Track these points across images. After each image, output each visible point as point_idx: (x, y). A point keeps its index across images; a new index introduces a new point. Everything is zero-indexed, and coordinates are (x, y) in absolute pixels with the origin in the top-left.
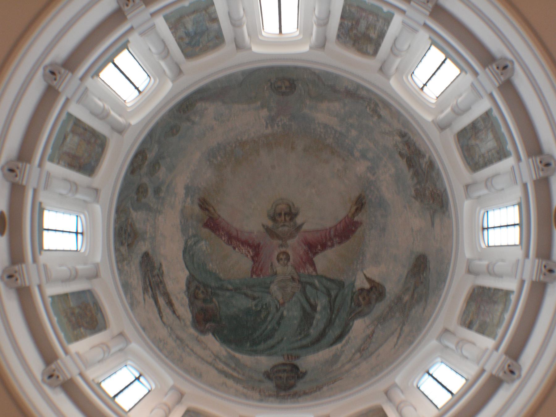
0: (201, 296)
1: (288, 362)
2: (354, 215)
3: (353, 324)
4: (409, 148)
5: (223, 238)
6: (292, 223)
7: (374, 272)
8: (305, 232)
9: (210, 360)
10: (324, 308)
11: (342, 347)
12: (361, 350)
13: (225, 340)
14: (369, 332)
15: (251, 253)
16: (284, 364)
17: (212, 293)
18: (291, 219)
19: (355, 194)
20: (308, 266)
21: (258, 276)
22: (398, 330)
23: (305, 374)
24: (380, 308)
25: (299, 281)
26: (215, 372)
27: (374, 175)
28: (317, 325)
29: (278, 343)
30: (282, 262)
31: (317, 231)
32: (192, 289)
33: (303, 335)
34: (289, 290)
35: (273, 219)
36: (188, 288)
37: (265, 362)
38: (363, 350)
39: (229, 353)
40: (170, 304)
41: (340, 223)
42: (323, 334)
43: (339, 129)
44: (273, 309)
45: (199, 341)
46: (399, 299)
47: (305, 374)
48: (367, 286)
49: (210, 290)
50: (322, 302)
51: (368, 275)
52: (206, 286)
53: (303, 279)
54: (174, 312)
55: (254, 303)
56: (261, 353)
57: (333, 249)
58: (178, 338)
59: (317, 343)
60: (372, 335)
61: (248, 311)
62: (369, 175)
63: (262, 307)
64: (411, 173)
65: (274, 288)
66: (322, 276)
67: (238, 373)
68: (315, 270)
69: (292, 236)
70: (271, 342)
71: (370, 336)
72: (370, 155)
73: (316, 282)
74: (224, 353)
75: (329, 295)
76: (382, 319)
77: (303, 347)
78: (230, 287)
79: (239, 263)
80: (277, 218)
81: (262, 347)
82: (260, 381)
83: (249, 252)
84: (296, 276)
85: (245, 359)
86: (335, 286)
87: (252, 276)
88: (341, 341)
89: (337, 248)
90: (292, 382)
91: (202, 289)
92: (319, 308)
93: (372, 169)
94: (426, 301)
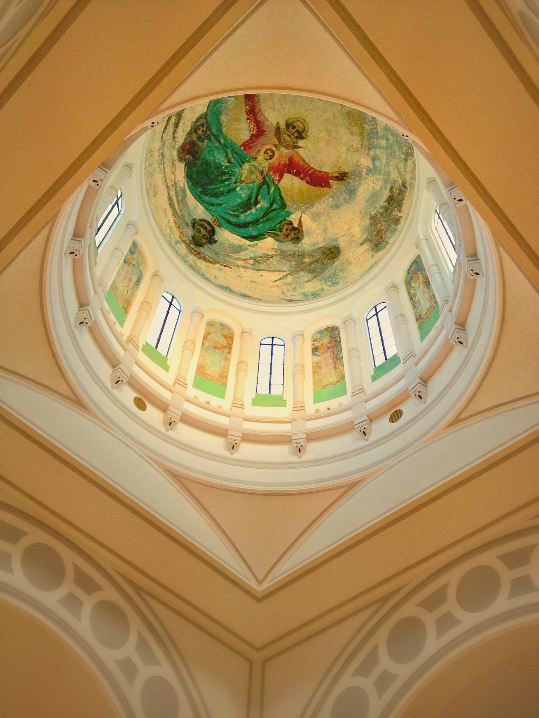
0: (200, 132)
1: (212, 223)
2: (331, 178)
3: (267, 237)
4: (399, 194)
5: (247, 107)
6: (295, 140)
7: (308, 223)
8: (297, 153)
9: (170, 184)
10: (261, 208)
11: (249, 246)
12: (256, 260)
13: (189, 176)
14: (270, 253)
15: (254, 132)
16: (209, 224)
17: (208, 135)
18: (297, 138)
19: (346, 169)
20: (278, 174)
21: (245, 150)
22: (285, 274)
23: (215, 242)
24: (289, 247)
25: (264, 177)
26: (166, 196)
27: (367, 174)
28: (248, 216)
29: (218, 205)
30: (266, 155)
31: (304, 161)
32: (199, 123)
33: (235, 213)
34: (253, 177)
35: (288, 125)
36: (197, 121)
37: (199, 211)
38: (258, 261)
39: (184, 186)
40: (177, 125)
41: (320, 172)
42: (245, 225)
43: (379, 130)
44: (233, 179)
45: (173, 164)
46: (302, 255)
47: (215, 242)
48: (296, 225)
49: (208, 132)
50: (263, 204)
51: (302, 219)
52: (208, 128)
53: (267, 178)
54: (174, 133)
55: (227, 164)
56: (202, 202)
57: (301, 181)
58: (162, 154)
59: (239, 227)
60: (270, 258)
61: (218, 167)
62: (364, 170)
63: (229, 172)
64: (384, 204)
65: (246, 166)
66: (279, 189)
67: (179, 206)
68: (279, 181)
69: (286, 147)
70: (214, 200)
71: (269, 257)
72: (377, 164)
73: (273, 189)
74: (182, 185)
75: (271, 205)
76: (284, 255)
77: (228, 222)
78: (222, 141)
79: (240, 131)
80: (290, 128)
81: (207, 198)
82: (187, 224)
83: (254, 130)
84: (265, 173)
85: (191, 199)
86: (280, 204)
87: (241, 146)
88: (251, 241)
89: (303, 183)
90: (204, 241)
91: (204, 128)
92: (259, 206)
93: (369, 171)
94: (314, 277)
